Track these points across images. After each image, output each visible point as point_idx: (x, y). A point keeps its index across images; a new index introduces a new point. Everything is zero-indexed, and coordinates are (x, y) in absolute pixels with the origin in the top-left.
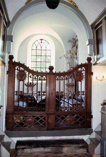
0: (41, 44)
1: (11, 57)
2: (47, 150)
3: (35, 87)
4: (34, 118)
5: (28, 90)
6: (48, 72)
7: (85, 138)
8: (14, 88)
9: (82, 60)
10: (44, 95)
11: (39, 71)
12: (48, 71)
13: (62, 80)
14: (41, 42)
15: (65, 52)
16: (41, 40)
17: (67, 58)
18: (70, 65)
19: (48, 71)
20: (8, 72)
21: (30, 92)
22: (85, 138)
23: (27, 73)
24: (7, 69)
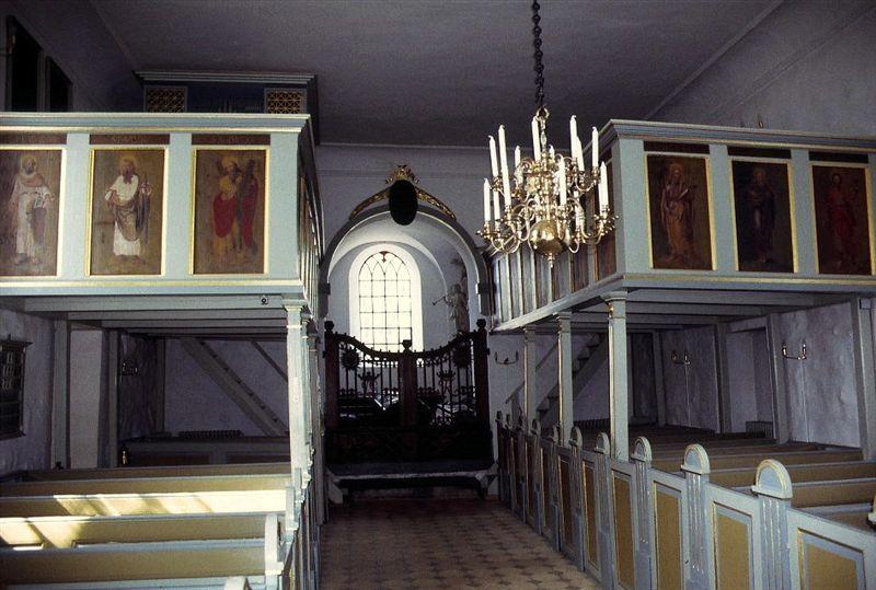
0: (385, 265)
1: (329, 325)
2: (403, 491)
3: (378, 380)
4: (682, 253)
5: (365, 388)
6: (401, 351)
7: (479, 475)
8: (338, 383)
9: (473, 327)
10: (395, 395)
11: (384, 350)
12: (402, 349)
13: (437, 364)
14: (384, 260)
15: (446, 289)
16: (384, 253)
17: (451, 304)
18: (457, 322)
19: (402, 349)
20: (325, 354)
21: (369, 390)
22: (479, 475)
23: (361, 354)
24: (322, 347)
